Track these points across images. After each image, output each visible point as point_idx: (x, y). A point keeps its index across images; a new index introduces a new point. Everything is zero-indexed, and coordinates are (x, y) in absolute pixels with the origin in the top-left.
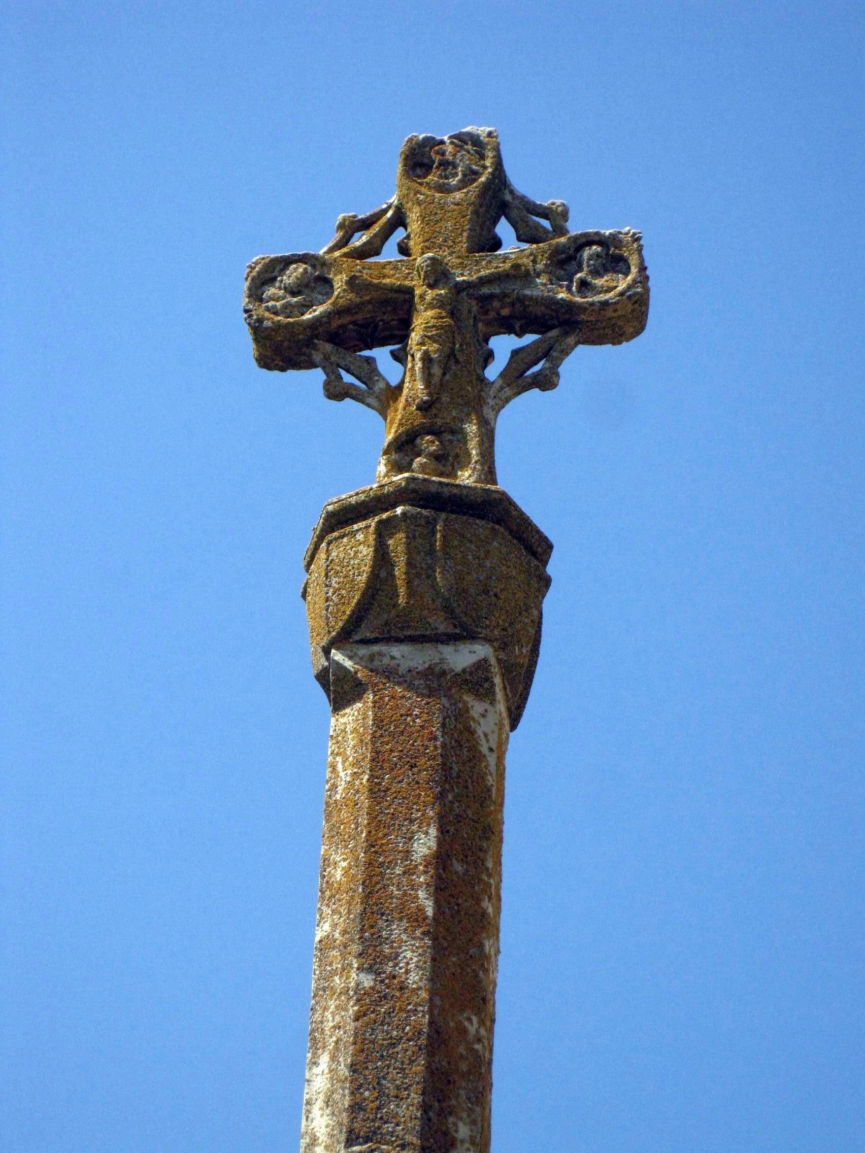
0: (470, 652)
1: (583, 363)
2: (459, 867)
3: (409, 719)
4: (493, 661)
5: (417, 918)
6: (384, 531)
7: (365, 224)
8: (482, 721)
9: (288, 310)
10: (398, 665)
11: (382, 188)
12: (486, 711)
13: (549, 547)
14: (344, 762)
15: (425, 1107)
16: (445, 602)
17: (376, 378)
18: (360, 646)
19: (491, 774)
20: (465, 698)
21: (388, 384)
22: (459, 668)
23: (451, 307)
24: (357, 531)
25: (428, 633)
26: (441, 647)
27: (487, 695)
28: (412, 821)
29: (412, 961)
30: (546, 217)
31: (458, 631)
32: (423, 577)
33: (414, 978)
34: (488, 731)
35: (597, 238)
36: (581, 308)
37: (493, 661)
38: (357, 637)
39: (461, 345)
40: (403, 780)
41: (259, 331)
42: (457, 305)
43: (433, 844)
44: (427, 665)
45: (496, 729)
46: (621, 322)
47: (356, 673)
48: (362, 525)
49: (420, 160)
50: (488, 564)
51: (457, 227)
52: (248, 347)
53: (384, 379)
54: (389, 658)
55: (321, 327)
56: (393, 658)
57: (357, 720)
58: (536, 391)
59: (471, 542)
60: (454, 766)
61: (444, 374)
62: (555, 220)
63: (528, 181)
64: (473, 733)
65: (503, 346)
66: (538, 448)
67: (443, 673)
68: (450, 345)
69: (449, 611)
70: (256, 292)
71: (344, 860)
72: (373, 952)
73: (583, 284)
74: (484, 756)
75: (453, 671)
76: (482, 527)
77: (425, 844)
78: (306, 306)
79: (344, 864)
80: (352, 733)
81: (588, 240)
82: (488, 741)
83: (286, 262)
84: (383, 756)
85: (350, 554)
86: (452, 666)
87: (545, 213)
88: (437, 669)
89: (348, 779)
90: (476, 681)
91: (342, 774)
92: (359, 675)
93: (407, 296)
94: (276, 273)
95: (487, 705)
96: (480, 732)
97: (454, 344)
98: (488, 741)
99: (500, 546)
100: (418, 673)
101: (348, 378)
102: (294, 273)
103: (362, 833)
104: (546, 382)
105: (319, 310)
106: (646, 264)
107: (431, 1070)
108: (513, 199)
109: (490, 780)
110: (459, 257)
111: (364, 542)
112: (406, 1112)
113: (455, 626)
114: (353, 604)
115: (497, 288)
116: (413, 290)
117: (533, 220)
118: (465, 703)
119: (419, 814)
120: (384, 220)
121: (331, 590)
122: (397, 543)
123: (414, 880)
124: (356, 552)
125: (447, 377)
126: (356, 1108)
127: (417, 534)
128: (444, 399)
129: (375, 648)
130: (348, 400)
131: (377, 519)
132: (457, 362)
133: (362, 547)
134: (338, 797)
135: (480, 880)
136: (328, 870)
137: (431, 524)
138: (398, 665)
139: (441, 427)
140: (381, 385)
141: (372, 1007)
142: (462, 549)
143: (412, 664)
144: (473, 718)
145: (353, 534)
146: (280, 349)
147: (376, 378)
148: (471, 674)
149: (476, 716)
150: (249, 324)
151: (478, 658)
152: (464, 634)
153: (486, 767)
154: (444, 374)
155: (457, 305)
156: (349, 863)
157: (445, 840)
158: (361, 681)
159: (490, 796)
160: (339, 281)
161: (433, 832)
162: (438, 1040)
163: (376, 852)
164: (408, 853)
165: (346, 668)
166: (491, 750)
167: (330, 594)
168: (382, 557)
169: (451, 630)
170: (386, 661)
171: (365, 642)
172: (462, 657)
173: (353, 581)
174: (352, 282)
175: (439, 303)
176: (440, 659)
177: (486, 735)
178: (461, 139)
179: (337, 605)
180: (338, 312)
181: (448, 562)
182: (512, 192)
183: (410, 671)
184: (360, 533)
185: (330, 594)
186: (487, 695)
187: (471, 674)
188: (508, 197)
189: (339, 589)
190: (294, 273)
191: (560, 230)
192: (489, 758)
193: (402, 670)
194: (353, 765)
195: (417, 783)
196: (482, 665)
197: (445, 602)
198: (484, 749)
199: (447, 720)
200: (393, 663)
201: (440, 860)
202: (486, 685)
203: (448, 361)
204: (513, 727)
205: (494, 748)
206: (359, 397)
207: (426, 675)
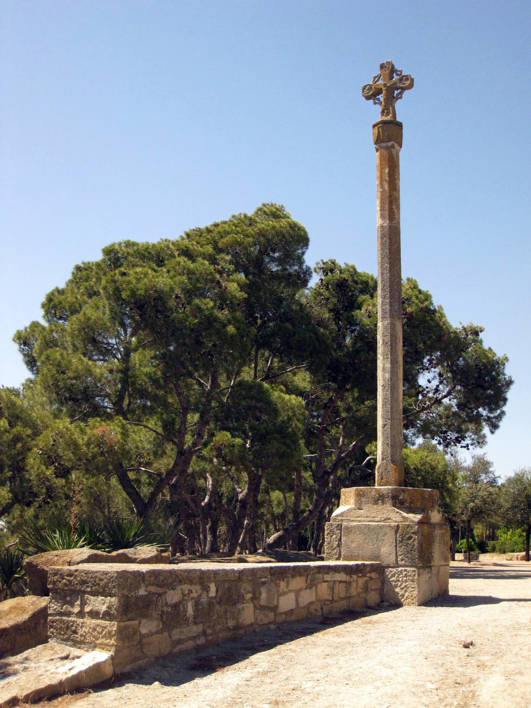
1: (406, 92)
5: (387, 181)
6: (379, 128)
7: (377, 77)
9: (367, 93)
11: (378, 72)
13: (401, 123)
15: (389, 206)
16: (389, 135)
23: (387, 90)
29: (386, 187)
33: (387, 189)
42: (389, 87)
46: (411, 86)
49: (382, 66)
51: (387, 77)
52: (364, 99)
55: (372, 94)
63: (397, 67)
65: (396, 92)
70: (363, 92)
72: (382, 186)
76: (390, 125)
77: (387, 171)
78: (369, 92)
81: (404, 76)
83: (366, 86)
84: (381, 156)
87: (399, 71)
90: (393, 146)
101: (376, 101)
102: (368, 87)
105: (371, 92)
106: (373, 157)
107: (389, 201)
109: (396, 159)
112: (387, 206)
117: (399, 73)
122: (380, 130)
126: (381, 207)
137: (384, 126)
141: (382, 193)
146: (368, 98)
150: (364, 96)
152: (390, 141)
155: (389, 87)
160: (373, 88)
162: (390, 196)
168: (379, 132)
172: (390, 144)
174: (375, 88)
175: (385, 90)
178: (387, 62)
180: (373, 92)
190: (368, 87)
191: (401, 74)
197: (389, 135)
201: (389, 172)
206: (378, 104)
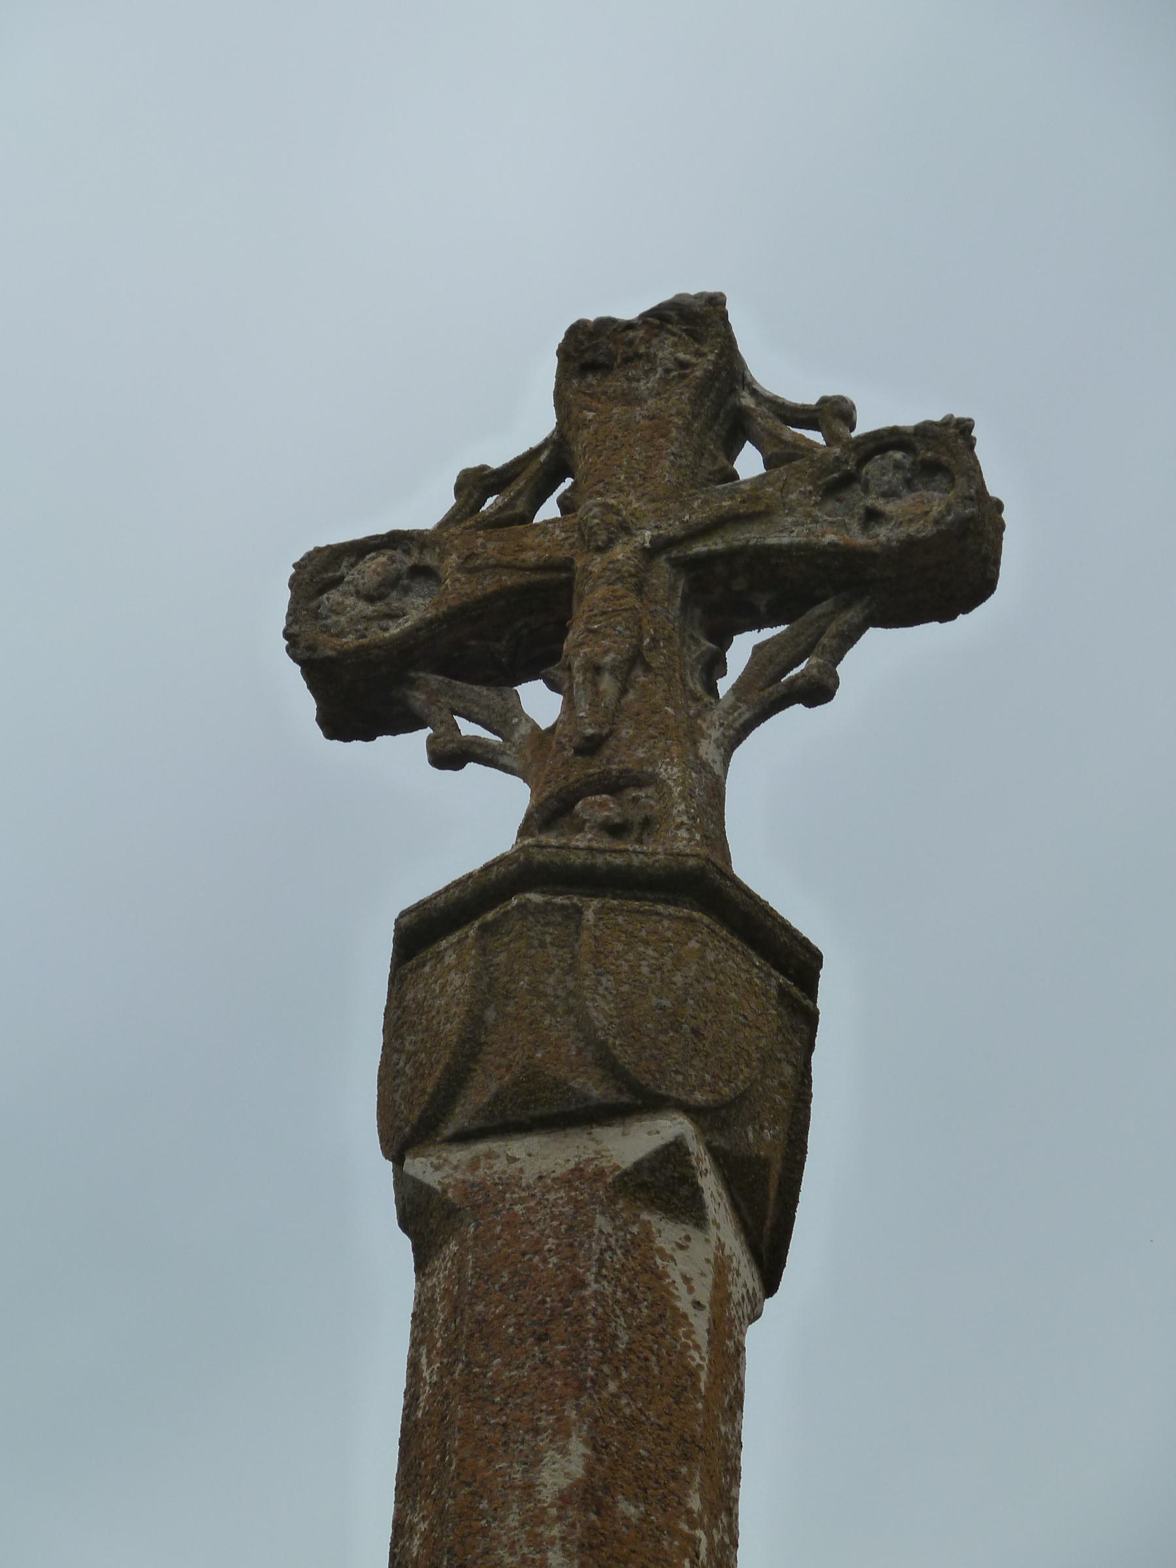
0: (649, 1133)
2: (628, 1509)
3: (537, 1258)
4: (696, 1147)
8: (679, 1255)
10: (521, 1171)
12: (688, 1238)
14: (429, 1352)
17: (515, 720)
18: (454, 1148)
19: (697, 1347)
20: (645, 1216)
21: (536, 727)
22: (627, 1163)
24: (446, 949)
25: (573, 1107)
26: (598, 1132)
27: (689, 1209)
28: (536, 1431)
30: (813, 425)
31: (625, 1099)
32: (560, 1010)
34: (692, 1271)
35: (894, 439)
36: (866, 555)
37: (696, 1147)
38: (449, 1130)
39: (653, 639)
40: (524, 1364)
41: (320, 671)
43: (577, 1468)
44: (572, 1165)
45: (709, 1269)
47: (445, 1191)
48: (453, 938)
50: (678, 978)
53: (528, 719)
54: (503, 1159)
56: (512, 1160)
57: (450, 1276)
58: (798, 709)
59: (647, 943)
60: (621, 1333)
61: (624, 692)
62: (828, 427)
64: (661, 1276)
66: (796, 804)
67: (600, 1174)
68: (634, 641)
69: (607, 1063)
71: (424, 1518)
73: (872, 516)
74: (685, 1316)
75: (618, 1167)
76: (668, 917)
79: (423, 1526)
80: (442, 1299)
82: (691, 1290)
85: (434, 991)
86: (616, 1160)
88: (590, 1169)
89: (435, 1378)
91: (426, 1374)
92: (450, 1195)
93: (564, 575)
94: (343, 570)
95: (690, 1230)
96: (675, 1275)
97: (641, 640)
98: (691, 1290)
99: (706, 946)
100: (554, 1180)
101: (468, 728)
103: (450, 1464)
104: (818, 691)
108: (758, 404)
110: (653, 501)
111: (455, 967)
113: (620, 1091)
114: (437, 1074)
115: (719, 541)
116: (572, 561)
118: (646, 1225)
119: (552, 1419)
120: (534, 467)
121: (404, 1057)
123: (540, 1535)
124: (443, 987)
125: (631, 696)
127: (548, 939)
128: (623, 733)
129: (481, 1147)
130: (471, 766)
131: (477, 924)
132: (648, 669)
133: (452, 974)
134: (420, 1414)
135: (674, 1533)
136: (401, 1543)
138: (521, 1171)
139: (618, 778)
140: (524, 729)
142: (630, 956)
143: (545, 1166)
144: (661, 1251)
145: (439, 956)
147: (515, 720)
148: (652, 1171)
149: (668, 1248)
151: (663, 1142)
152: (644, 1102)
153: (687, 1335)
154: (624, 692)
156: (431, 1524)
157: (600, 1460)
158: (453, 1205)
159: (694, 1384)
161: (577, 1447)
163: (473, 1493)
164: (529, 1489)
165: (429, 1187)
166: (697, 1305)
167: (401, 1064)
169: (613, 1097)
170: (500, 1165)
171: (463, 1138)
172: (631, 1144)
173: (437, 1034)
176: (597, 1152)
177: (687, 1280)
179: (411, 1080)
181: (604, 980)
182: (755, 393)
183: (540, 1178)
184: (450, 952)
185: (401, 1064)
186: (689, 1209)
187: (652, 1171)
188: (748, 401)
189: (415, 1053)
192: (692, 1320)
193: (529, 1178)
194: (441, 1353)
195: (550, 1365)
196: (675, 1151)
198: (684, 1304)
199: (607, 1255)
200: (512, 1169)
202: (684, 1191)
203: (630, 669)
204: (770, 1285)
205: (705, 1301)
207: (569, 1181)
